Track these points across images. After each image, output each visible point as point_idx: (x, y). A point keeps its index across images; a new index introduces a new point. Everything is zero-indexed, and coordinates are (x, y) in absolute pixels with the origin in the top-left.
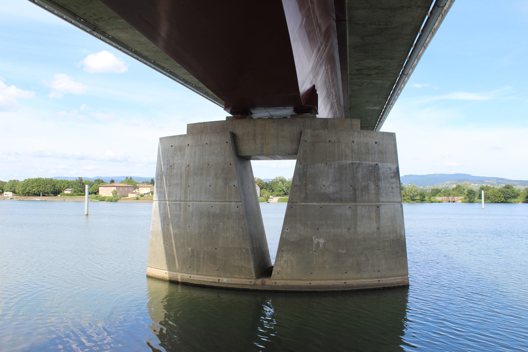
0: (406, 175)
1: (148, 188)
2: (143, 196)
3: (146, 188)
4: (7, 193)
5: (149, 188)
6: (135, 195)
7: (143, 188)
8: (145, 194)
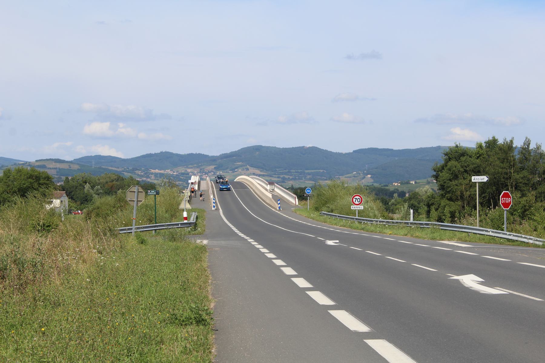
0: (191, 155)
4: (417, 190)
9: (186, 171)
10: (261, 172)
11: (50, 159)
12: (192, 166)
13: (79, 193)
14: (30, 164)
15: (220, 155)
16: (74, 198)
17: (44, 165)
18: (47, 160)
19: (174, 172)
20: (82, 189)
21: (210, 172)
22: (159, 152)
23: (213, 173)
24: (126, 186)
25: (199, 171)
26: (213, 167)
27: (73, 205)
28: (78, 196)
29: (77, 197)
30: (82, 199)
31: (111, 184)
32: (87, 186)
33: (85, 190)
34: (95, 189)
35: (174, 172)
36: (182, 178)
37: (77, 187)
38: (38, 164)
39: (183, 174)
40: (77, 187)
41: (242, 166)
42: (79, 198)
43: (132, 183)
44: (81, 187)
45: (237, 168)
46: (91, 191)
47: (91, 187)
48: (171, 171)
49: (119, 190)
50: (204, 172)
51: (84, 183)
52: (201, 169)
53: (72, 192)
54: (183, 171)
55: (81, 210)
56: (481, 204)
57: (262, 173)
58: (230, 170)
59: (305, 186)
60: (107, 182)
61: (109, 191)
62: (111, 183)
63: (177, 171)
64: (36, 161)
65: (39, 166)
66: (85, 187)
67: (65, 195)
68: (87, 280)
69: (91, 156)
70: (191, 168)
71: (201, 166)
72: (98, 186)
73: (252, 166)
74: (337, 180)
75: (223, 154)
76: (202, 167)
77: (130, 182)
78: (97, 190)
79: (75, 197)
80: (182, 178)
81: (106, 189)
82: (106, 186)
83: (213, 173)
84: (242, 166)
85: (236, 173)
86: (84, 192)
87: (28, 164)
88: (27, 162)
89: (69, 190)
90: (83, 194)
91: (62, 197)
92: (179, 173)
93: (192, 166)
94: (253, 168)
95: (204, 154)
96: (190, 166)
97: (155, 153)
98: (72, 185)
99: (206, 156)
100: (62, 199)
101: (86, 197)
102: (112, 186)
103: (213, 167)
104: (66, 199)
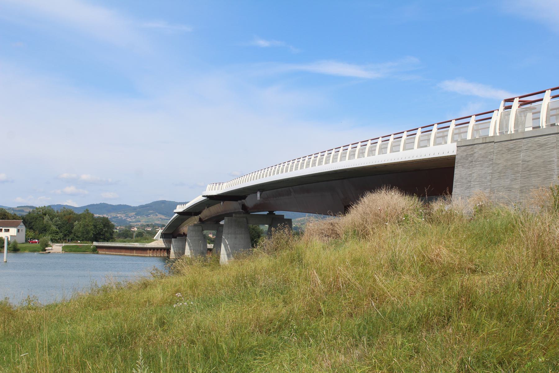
9: (117, 215)
10: (165, 217)
11: (27, 206)
12: (120, 213)
13: (39, 224)
15: (139, 206)
16: (34, 228)
17: (23, 210)
18: (25, 206)
19: (108, 216)
20: (41, 220)
21: (132, 217)
22: (99, 203)
23: (134, 217)
24: (82, 219)
25: (125, 216)
26: (134, 213)
27: (32, 234)
28: (37, 226)
29: (37, 228)
30: (41, 229)
32: (46, 218)
34: (53, 220)
35: (108, 216)
36: (114, 220)
38: (18, 209)
39: (114, 217)
40: (37, 218)
41: (152, 213)
42: (39, 228)
43: (88, 215)
44: (40, 218)
45: (149, 214)
46: (50, 222)
47: (50, 219)
48: (106, 215)
49: (75, 221)
50: (128, 217)
51: (44, 215)
52: (126, 215)
53: (32, 222)
54: (114, 216)
55: (38, 240)
57: (166, 218)
58: (146, 216)
59: (453, 194)
60: (65, 215)
61: (66, 223)
62: (68, 216)
63: (111, 216)
64: (18, 207)
65: (19, 211)
66: (45, 218)
67: (22, 224)
69: (54, 205)
70: (120, 214)
71: (126, 212)
72: (56, 218)
73: (159, 213)
75: (140, 206)
76: (127, 214)
77: (86, 215)
79: (34, 227)
80: (114, 220)
81: (64, 220)
83: (134, 217)
84: (152, 213)
85: (149, 217)
86: (43, 223)
87: (12, 209)
88: (11, 208)
89: (29, 220)
90: (43, 225)
91: (19, 226)
92: (112, 217)
93: (120, 213)
94: (160, 215)
95: (128, 205)
96: (119, 213)
97: (96, 204)
98: (33, 217)
99: (130, 207)
100: (19, 227)
101: (45, 227)
102: (70, 218)
103: (134, 213)
104: (23, 228)
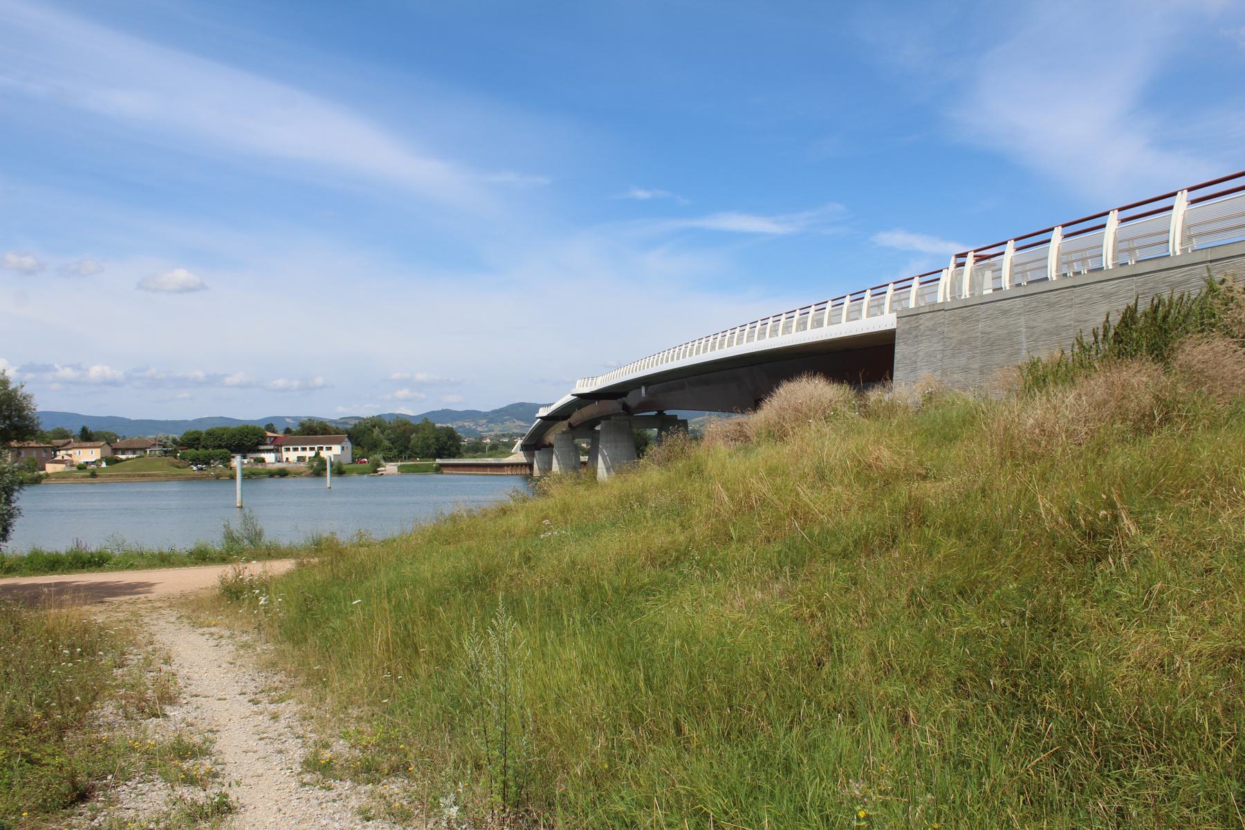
1: (94, 450)
2: (85, 468)
3: (89, 450)
5: (99, 450)
6: (64, 466)
7: (81, 451)
8: (87, 462)
14: (335, 422)
27: (359, 452)
31: (403, 428)
32: (376, 431)
33: (374, 435)
37: (364, 432)
38: (341, 421)
39: (460, 427)
46: (381, 436)
56: (332, 472)
60: (399, 427)
65: (343, 423)
67: (347, 439)
68: (65, 651)
73: (517, 419)
74: (963, 333)
78: (388, 435)
82: (398, 431)
100: (344, 443)
104: (348, 445)
